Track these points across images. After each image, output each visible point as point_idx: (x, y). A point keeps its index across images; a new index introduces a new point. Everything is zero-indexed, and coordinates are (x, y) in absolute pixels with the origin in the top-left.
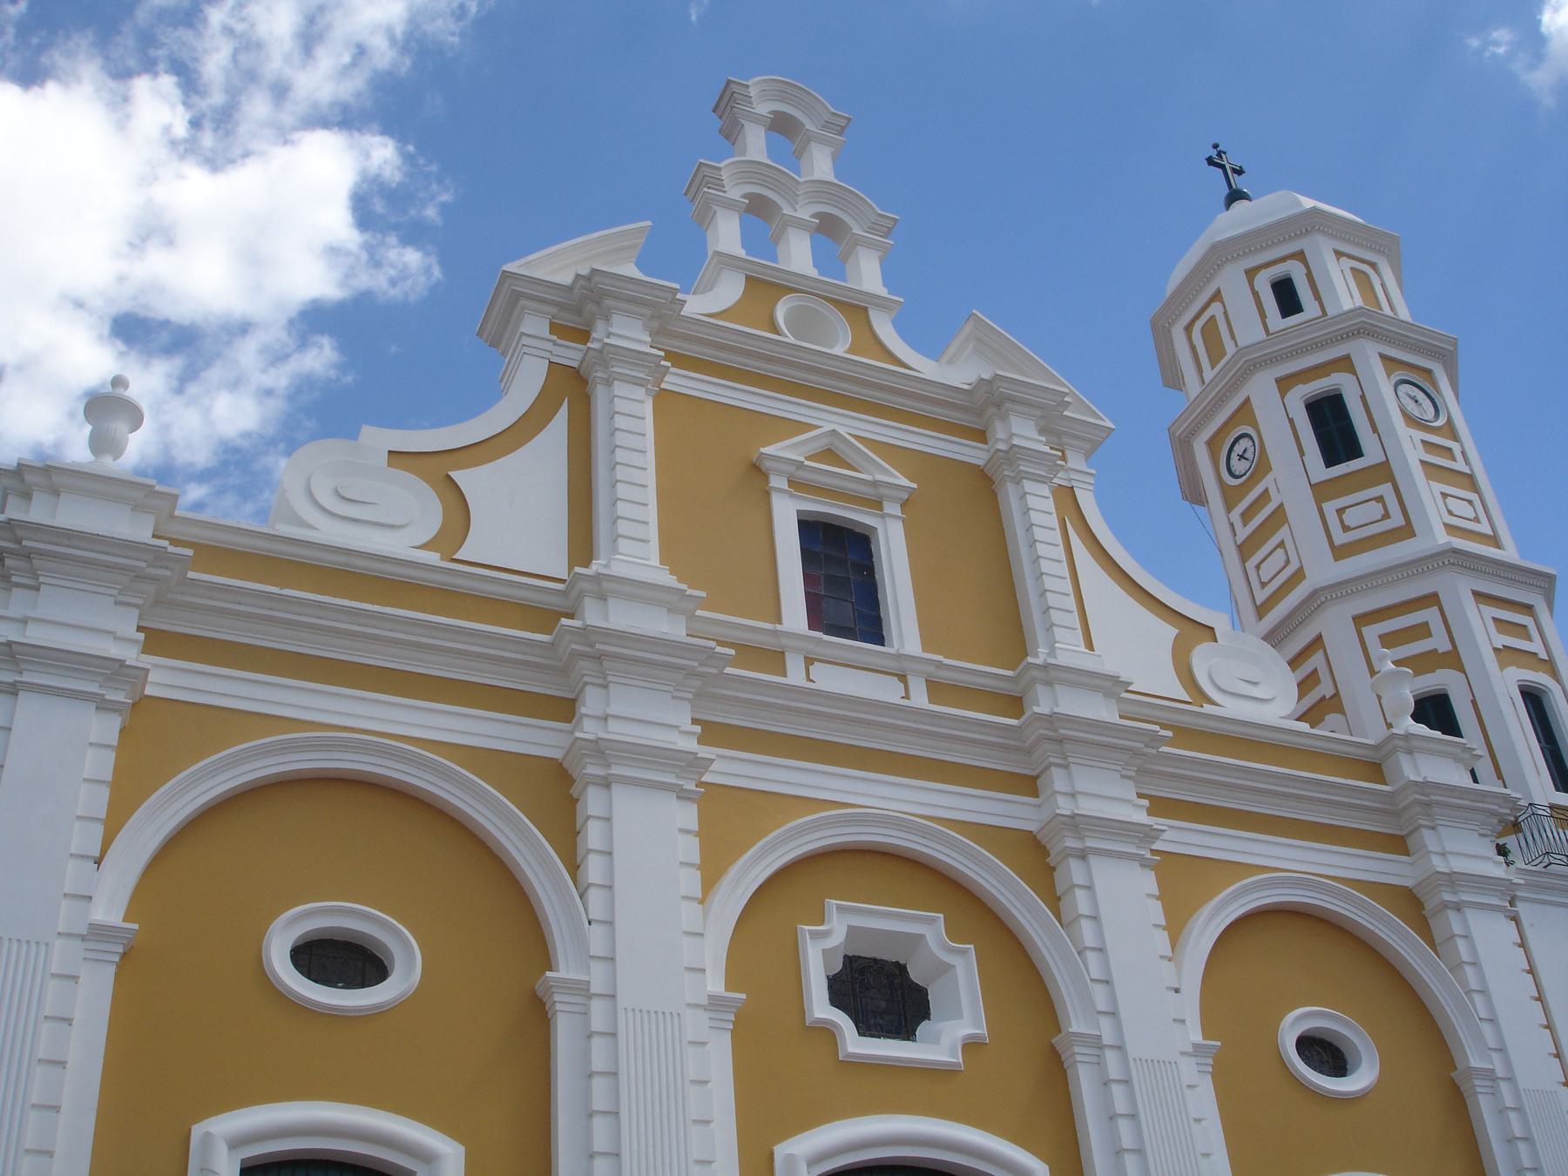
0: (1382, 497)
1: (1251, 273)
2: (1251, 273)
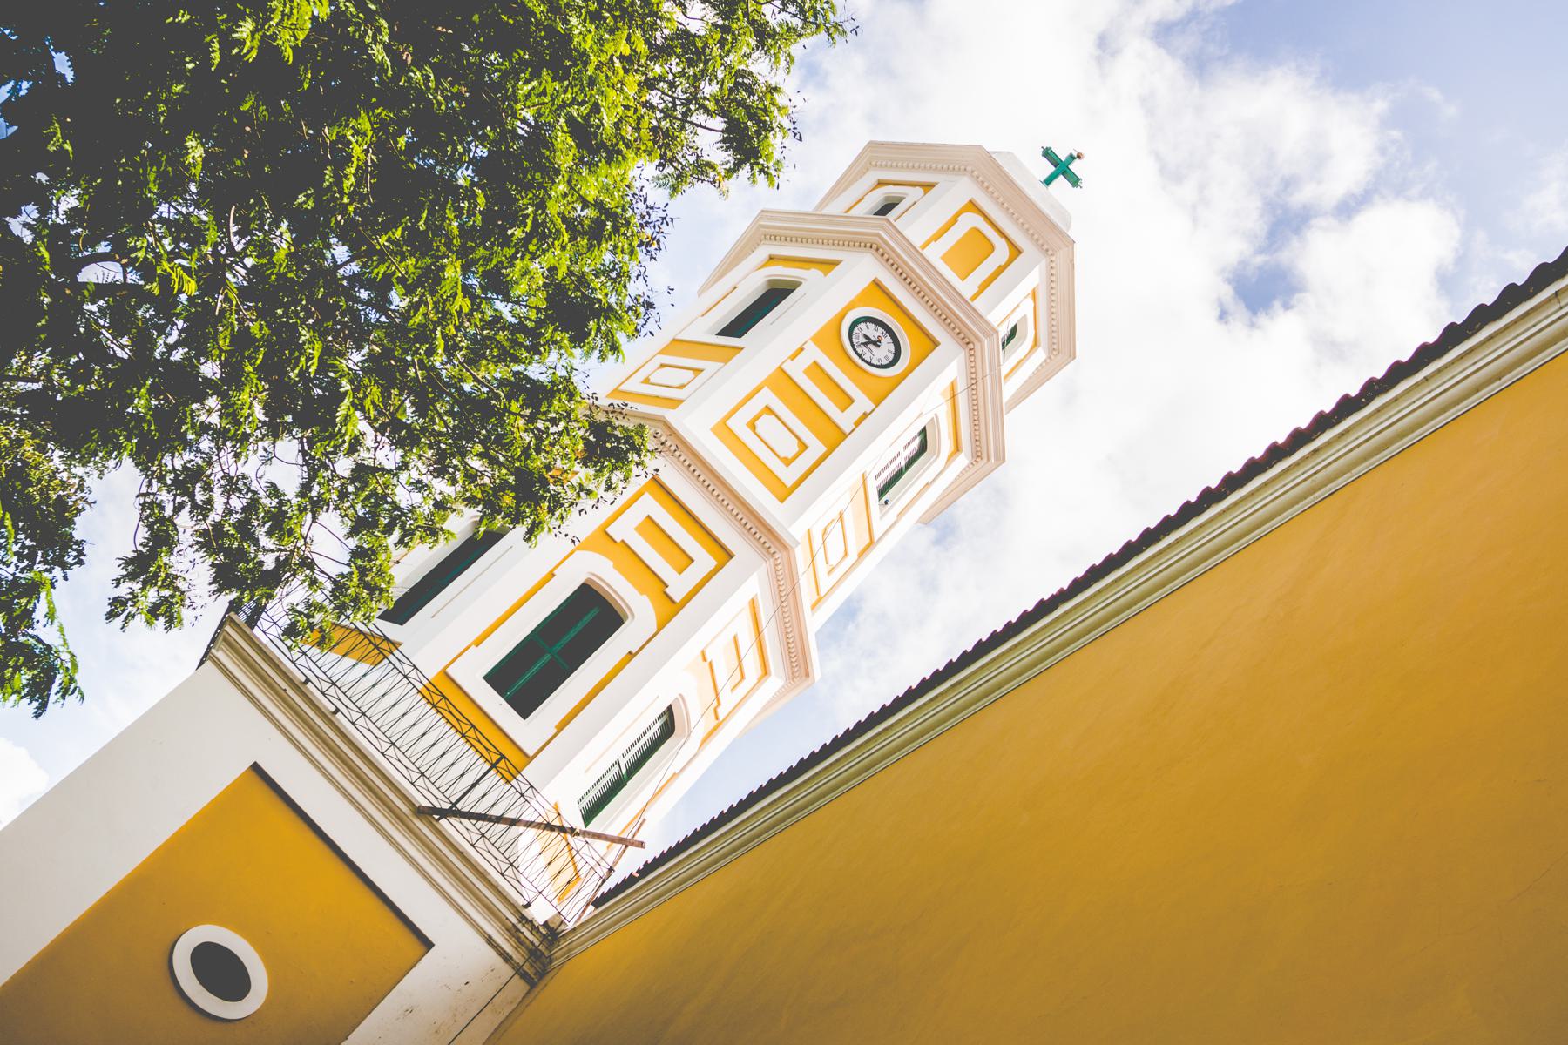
1: (973, 206)
2: (973, 206)
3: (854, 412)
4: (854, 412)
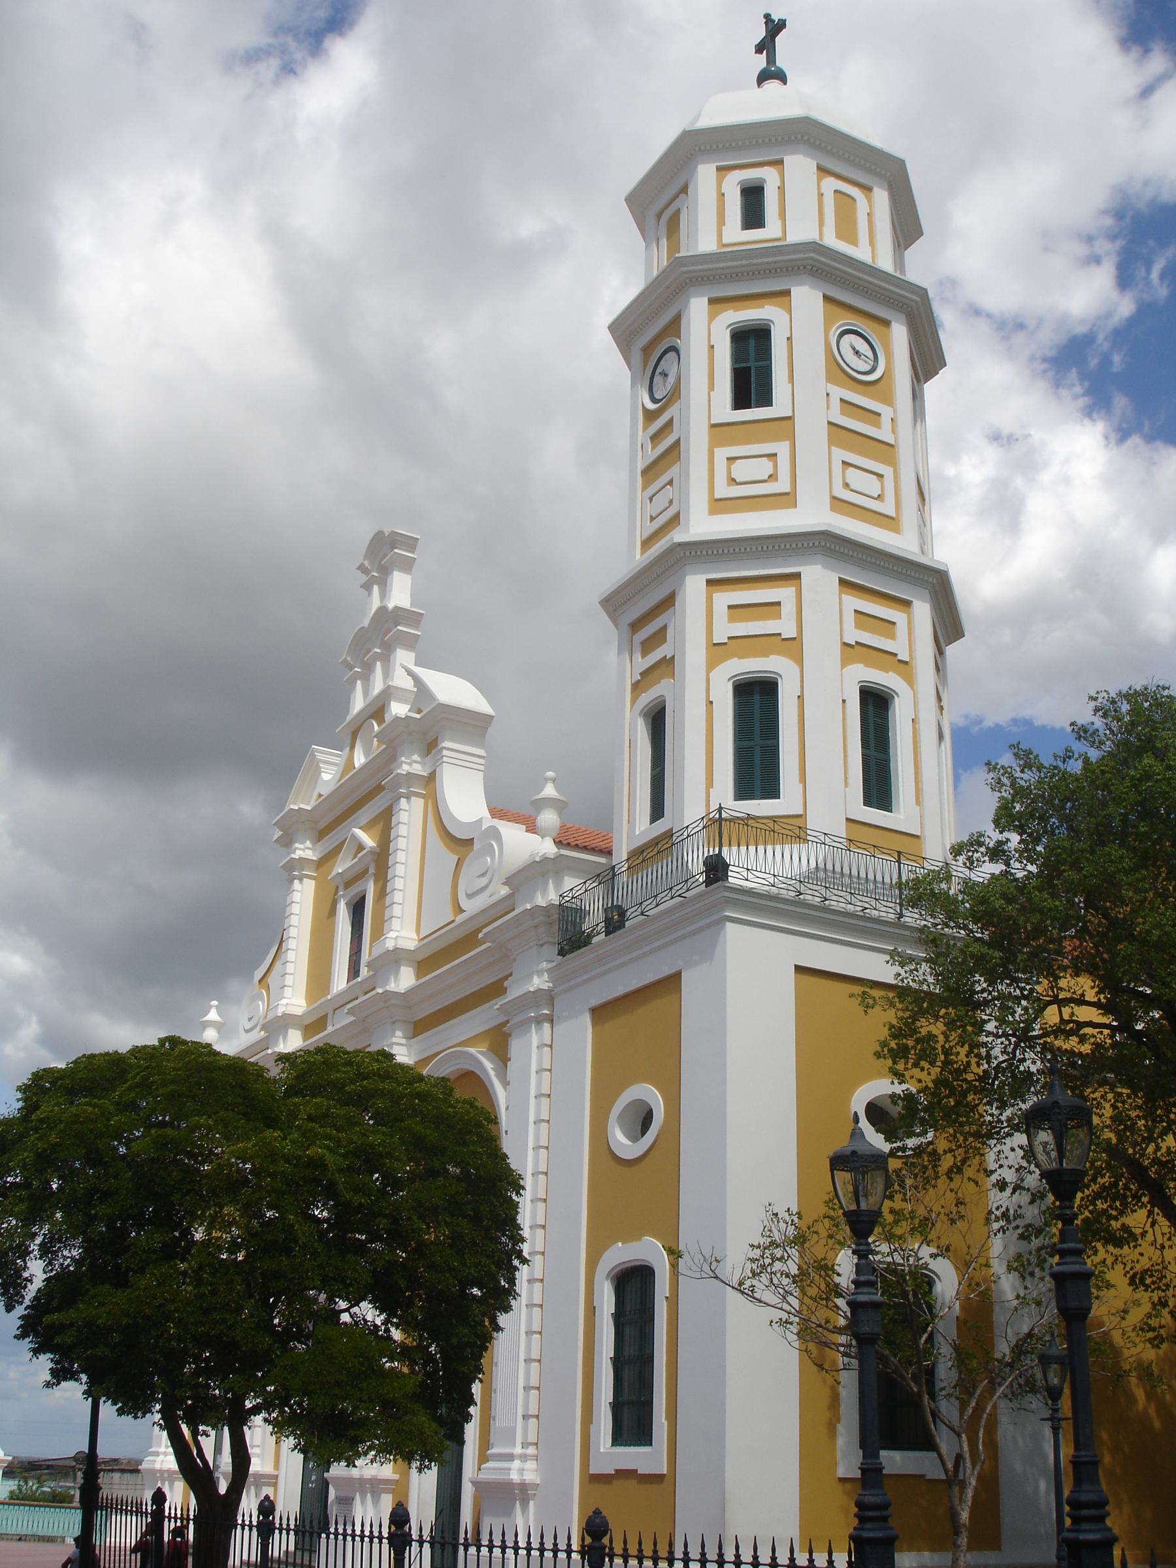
3: (788, 609)
4: (788, 609)
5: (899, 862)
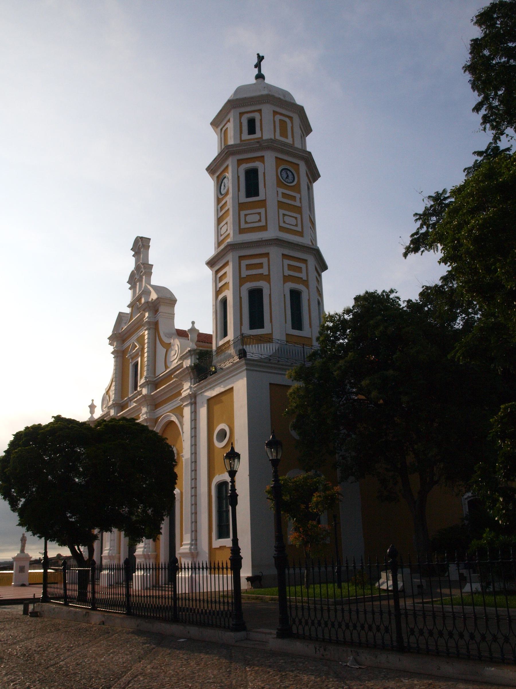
0: (260, 213)
1: (241, 114)
2: (241, 114)
5: (303, 347)
